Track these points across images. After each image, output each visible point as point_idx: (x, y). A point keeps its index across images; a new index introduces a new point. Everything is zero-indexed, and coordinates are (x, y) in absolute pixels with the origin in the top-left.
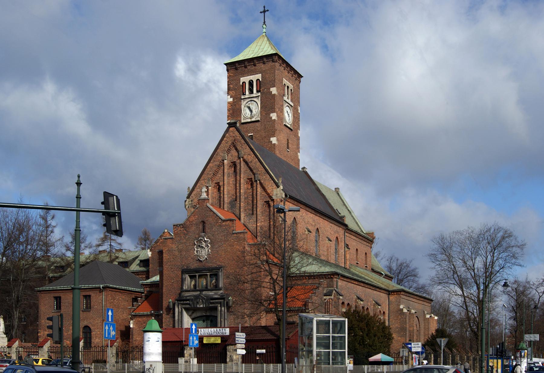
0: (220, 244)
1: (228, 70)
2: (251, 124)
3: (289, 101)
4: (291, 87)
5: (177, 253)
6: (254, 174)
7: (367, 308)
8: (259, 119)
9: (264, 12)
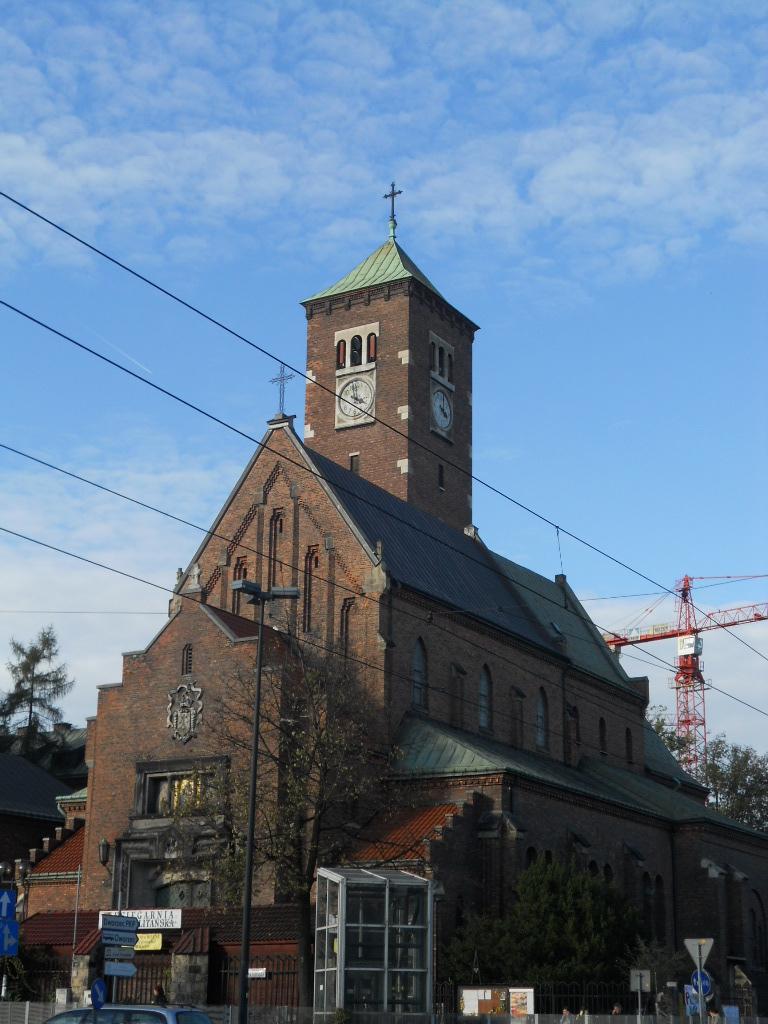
1: (310, 316)
2: (356, 430)
3: (444, 381)
4: (449, 348)
7: (607, 867)
9: (393, 194)
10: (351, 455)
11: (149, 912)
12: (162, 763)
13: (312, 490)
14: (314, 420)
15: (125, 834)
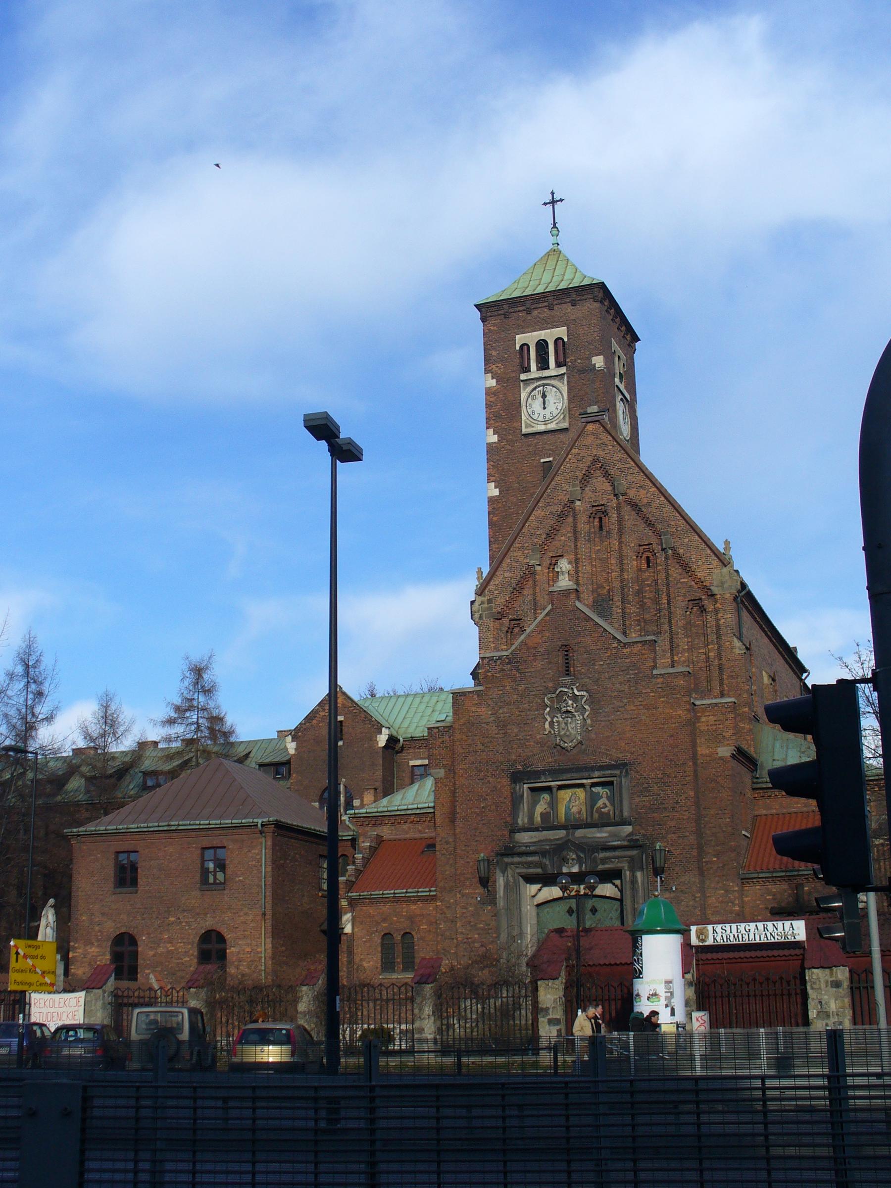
0: (617, 704)
1: (484, 319)
2: (545, 437)
4: (623, 356)
5: (493, 729)
6: (659, 535)
8: (565, 425)
9: (553, 202)
10: (542, 461)
11: (760, 925)
12: (543, 772)
13: (641, 487)
14: (497, 424)
15: (506, 848)
